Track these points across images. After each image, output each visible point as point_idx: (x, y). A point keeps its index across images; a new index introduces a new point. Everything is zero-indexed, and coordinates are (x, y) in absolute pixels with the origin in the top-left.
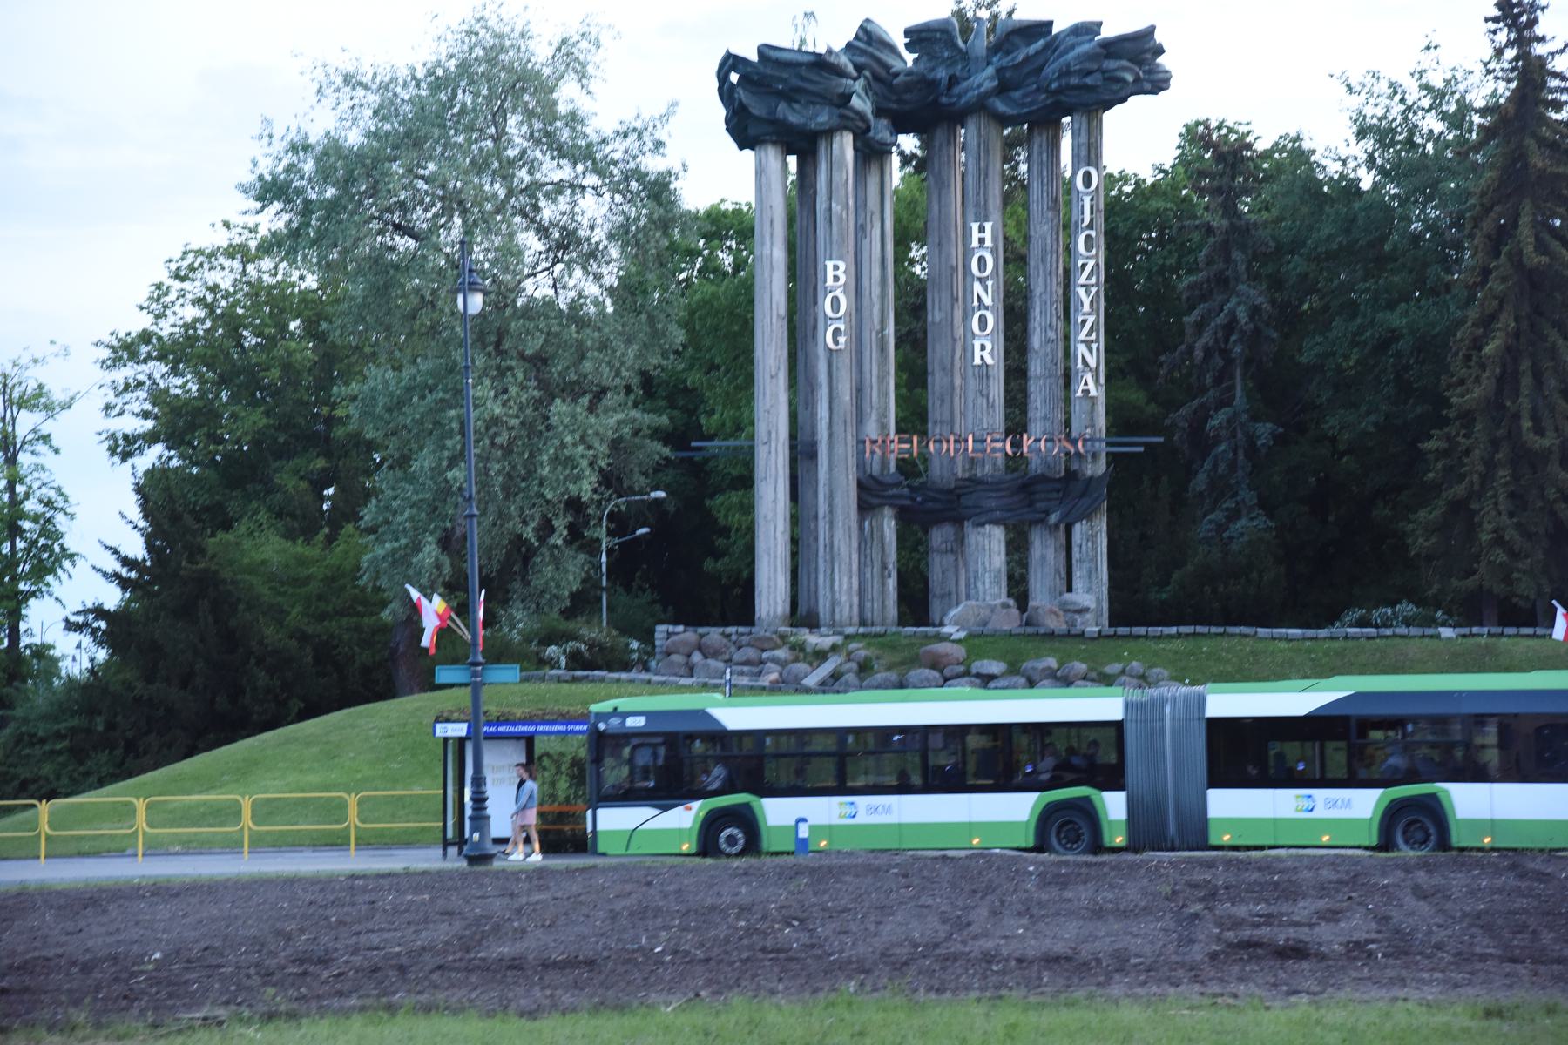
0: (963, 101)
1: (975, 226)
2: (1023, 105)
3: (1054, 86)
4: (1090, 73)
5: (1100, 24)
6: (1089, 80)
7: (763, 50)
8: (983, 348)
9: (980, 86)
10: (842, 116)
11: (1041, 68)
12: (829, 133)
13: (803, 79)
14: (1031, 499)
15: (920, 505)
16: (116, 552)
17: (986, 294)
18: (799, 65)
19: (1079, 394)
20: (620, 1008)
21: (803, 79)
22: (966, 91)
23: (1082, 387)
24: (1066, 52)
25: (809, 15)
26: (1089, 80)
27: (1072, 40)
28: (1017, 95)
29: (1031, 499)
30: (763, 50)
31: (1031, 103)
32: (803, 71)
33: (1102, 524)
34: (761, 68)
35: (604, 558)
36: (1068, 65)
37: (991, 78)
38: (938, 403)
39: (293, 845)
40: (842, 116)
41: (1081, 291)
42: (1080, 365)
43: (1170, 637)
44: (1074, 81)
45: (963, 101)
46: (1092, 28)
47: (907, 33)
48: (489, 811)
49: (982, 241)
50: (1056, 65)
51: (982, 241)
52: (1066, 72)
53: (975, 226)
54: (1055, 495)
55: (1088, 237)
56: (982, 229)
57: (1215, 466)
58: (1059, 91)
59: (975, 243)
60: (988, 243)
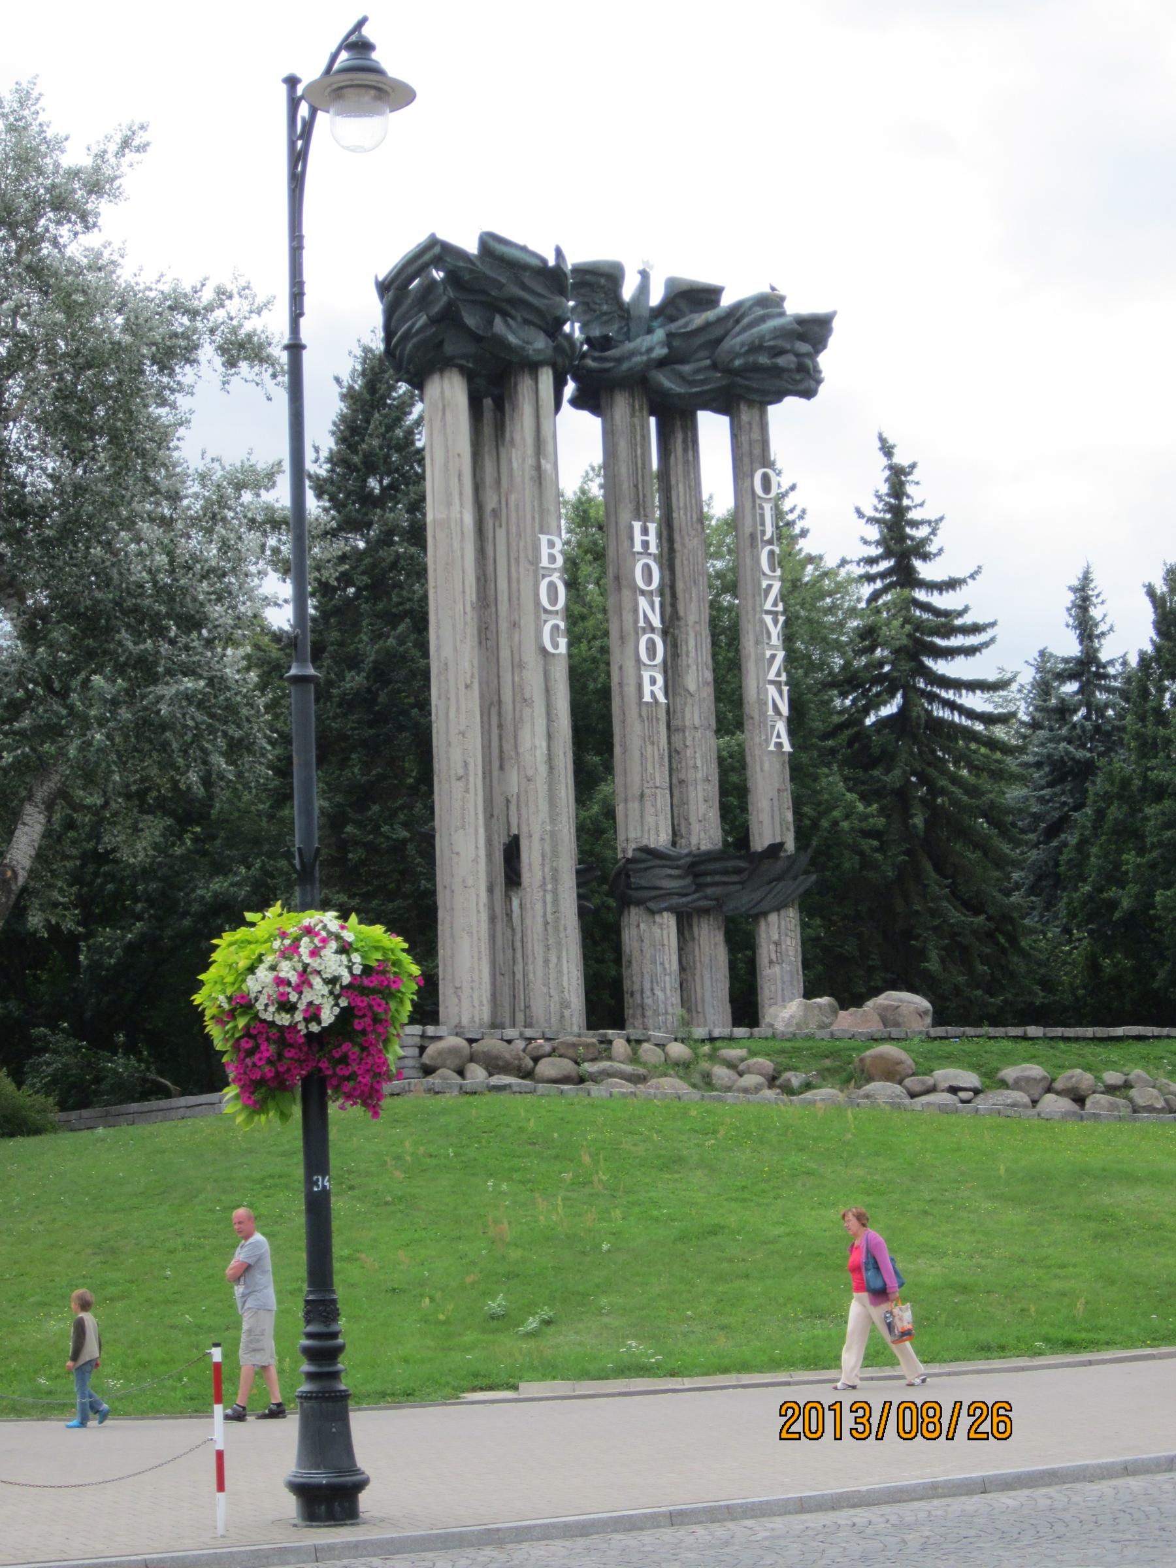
0: (625, 366)
1: (637, 526)
2: (692, 383)
3: (737, 363)
4: (781, 352)
5: (815, 331)
6: (781, 361)
7: (489, 243)
8: (653, 681)
9: (650, 350)
11: (719, 340)
13: (524, 287)
14: (721, 885)
15: (610, 888)
16: (898, 478)
17: (650, 611)
18: (525, 267)
19: (772, 748)
20: (44, 1419)
21: (524, 287)
22: (633, 354)
23: (774, 740)
24: (751, 325)
26: (781, 361)
28: (686, 368)
30: (489, 243)
31: (703, 382)
32: (527, 278)
33: (791, 916)
34: (478, 264)
35: (317, 875)
36: (762, 338)
39: (1069, 1345)
41: (768, 619)
42: (771, 712)
44: (763, 360)
45: (625, 366)
46: (770, 302)
49: (645, 544)
50: (745, 337)
51: (645, 544)
52: (756, 348)
53: (637, 526)
54: (735, 878)
55: (772, 553)
56: (645, 531)
57: (1059, 850)
59: (638, 547)
60: (653, 549)
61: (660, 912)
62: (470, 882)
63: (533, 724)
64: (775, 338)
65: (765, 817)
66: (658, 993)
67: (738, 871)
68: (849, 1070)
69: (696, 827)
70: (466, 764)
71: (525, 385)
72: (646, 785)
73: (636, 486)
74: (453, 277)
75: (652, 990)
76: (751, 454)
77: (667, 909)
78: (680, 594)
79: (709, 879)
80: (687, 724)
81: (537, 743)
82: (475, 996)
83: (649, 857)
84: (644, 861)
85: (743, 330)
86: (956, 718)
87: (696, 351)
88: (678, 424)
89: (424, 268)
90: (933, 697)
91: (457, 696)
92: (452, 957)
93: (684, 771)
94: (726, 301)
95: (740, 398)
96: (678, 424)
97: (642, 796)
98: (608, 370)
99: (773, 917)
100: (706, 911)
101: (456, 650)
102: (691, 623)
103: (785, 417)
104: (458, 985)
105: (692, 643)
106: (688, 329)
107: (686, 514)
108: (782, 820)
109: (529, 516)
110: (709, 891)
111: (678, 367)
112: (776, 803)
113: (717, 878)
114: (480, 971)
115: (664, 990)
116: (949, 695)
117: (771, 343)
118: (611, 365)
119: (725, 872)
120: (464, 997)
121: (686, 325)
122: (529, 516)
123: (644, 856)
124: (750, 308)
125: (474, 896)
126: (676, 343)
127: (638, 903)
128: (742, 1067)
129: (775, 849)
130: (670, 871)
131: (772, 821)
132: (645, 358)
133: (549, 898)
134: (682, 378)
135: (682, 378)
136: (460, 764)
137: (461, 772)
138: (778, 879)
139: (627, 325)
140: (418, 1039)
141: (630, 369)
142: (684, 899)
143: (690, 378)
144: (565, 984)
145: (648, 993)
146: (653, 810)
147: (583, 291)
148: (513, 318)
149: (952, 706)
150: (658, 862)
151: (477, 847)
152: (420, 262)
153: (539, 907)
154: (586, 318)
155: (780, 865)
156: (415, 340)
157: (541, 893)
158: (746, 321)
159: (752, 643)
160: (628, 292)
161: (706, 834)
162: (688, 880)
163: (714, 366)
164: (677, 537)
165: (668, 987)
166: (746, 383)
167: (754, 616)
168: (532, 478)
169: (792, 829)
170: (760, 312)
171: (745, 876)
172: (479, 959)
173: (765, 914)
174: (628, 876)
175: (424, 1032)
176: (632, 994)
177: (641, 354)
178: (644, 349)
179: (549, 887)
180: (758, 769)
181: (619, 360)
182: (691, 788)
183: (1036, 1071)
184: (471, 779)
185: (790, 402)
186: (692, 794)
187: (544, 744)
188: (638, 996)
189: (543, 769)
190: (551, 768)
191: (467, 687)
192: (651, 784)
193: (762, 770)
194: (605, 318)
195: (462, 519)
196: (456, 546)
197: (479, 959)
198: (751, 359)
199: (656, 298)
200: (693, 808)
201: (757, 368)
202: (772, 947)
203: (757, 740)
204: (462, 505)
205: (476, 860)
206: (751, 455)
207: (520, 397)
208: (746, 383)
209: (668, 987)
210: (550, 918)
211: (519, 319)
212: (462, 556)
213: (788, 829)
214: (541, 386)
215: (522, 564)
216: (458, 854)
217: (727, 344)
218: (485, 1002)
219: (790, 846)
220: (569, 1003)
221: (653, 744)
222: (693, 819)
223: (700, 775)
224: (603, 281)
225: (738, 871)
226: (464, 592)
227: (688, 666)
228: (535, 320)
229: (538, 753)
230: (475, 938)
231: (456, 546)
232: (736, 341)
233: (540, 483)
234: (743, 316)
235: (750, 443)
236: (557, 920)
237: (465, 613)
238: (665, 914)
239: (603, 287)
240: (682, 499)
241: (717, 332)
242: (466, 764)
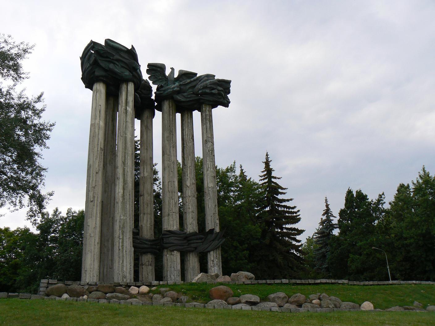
0: (166, 92)
4: (213, 89)
6: (213, 91)
7: (108, 42)
10: (133, 76)
11: (194, 86)
12: (127, 81)
25: (44, 159)
26: (213, 91)
27: (206, 78)
28: (185, 94)
29: (193, 244)
30: (108, 42)
32: (123, 54)
33: (219, 252)
37: (177, 87)
38: (146, 206)
40: (133, 76)
43: (310, 284)
44: (208, 91)
45: (166, 92)
47: (149, 65)
48: (229, 105)
50: (202, 84)
52: (205, 87)
54: (200, 241)
58: (202, 94)
61: (173, 251)
62: (92, 235)
63: (119, 185)
64: (211, 85)
65: (210, 223)
66: (172, 276)
67: (201, 239)
68: (203, 293)
69: (189, 226)
70: (94, 197)
71: (124, 87)
72: (170, 212)
73: (170, 126)
74: (97, 52)
75: (170, 276)
76: (206, 118)
77: (176, 250)
78: (185, 159)
79: (192, 241)
80: (187, 195)
81: (120, 191)
82: (91, 273)
83: (170, 233)
84: (168, 235)
85: (202, 83)
86: (285, 209)
87: (188, 90)
88: (186, 112)
89: (89, 50)
90: (279, 206)
91: (93, 175)
92: (85, 260)
93: (186, 209)
94: (198, 76)
95: (203, 103)
96: (186, 112)
97: (169, 215)
98: (161, 94)
99: (212, 253)
100: (192, 251)
101: (93, 162)
102: (188, 167)
103: (218, 112)
104: (86, 270)
105: (189, 172)
106: (185, 83)
107: (187, 136)
108: (215, 222)
109: (122, 123)
110: (192, 245)
111: (183, 94)
112: (213, 217)
113: (195, 241)
114: (94, 265)
115: (174, 276)
116: (283, 204)
117: (210, 86)
118: (162, 92)
119: (197, 239)
120: (88, 273)
121: (185, 82)
122: (122, 123)
123: (168, 233)
124: (204, 77)
125: (93, 240)
126: (182, 87)
127: (167, 248)
128: (165, 295)
129: (212, 231)
130: (177, 238)
131: (213, 222)
132: (172, 90)
133: (121, 241)
134: (184, 96)
135: (184, 96)
136: (92, 196)
137: (92, 200)
138: (213, 240)
139: (167, 83)
140: (46, 284)
141: (167, 93)
142: (182, 247)
143: (186, 97)
144: (125, 270)
145: (169, 277)
146: (172, 219)
147: (153, 72)
148: (118, 65)
149: (285, 207)
150: (172, 235)
151: (96, 224)
152: (88, 49)
153: (117, 244)
154: (155, 80)
155: (214, 236)
156: (87, 72)
157: (119, 239)
158: (202, 81)
159: (206, 171)
160: (168, 72)
161: (191, 226)
162: (185, 241)
163: (194, 93)
164: (185, 143)
165: (175, 274)
166: (203, 98)
167: (206, 162)
168: (124, 112)
169: (218, 225)
170: (206, 78)
171: (203, 240)
172: (94, 261)
173: (209, 252)
174: (163, 240)
175: (48, 282)
176: (165, 277)
177: (171, 89)
178: (171, 88)
179: (121, 237)
180: (207, 207)
181: (164, 91)
182: (188, 214)
183: (282, 295)
184: (96, 202)
185: (220, 107)
186: (188, 217)
187: (122, 191)
188: (166, 278)
189: (121, 199)
190: (124, 199)
191: (97, 173)
192: (172, 211)
193: (208, 208)
194: (161, 80)
195: (99, 123)
196: (97, 131)
197: (94, 261)
198: (204, 90)
199: (176, 75)
200: (188, 220)
201: (206, 94)
202: (212, 262)
203: (207, 199)
204: (100, 119)
205: (95, 228)
206: (207, 122)
207: (122, 90)
208: (203, 98)
209: (175, 274)
210: (120, 248)
211: (120, 66)
212: (98, 134)
213: (217, 225)
214: (129, 87)
215: (119, 137)
216: (89, 226)
217: (197, 87)
218: (95, 276)
219: (217, 230)
220: (126, 276)
221: (173, 199)
222: (188, 224)
223: (190, 210)
224: (159, 69)
225: (201, 239)
226: (98, 144)
227: (188, 179)
228: (126, 67)
229: (120, 194)
230: (93, 253)
231: (97, 131)
232: (200, 86)
233: (126, 114)
234: (201, 80)
235: (206, 115)
236: (123, 248)
237: (98, 151)
238: (175, 251)
239: (159, 71)
240: (186, 133)
241: (194, 84)
242: (94, 197)
